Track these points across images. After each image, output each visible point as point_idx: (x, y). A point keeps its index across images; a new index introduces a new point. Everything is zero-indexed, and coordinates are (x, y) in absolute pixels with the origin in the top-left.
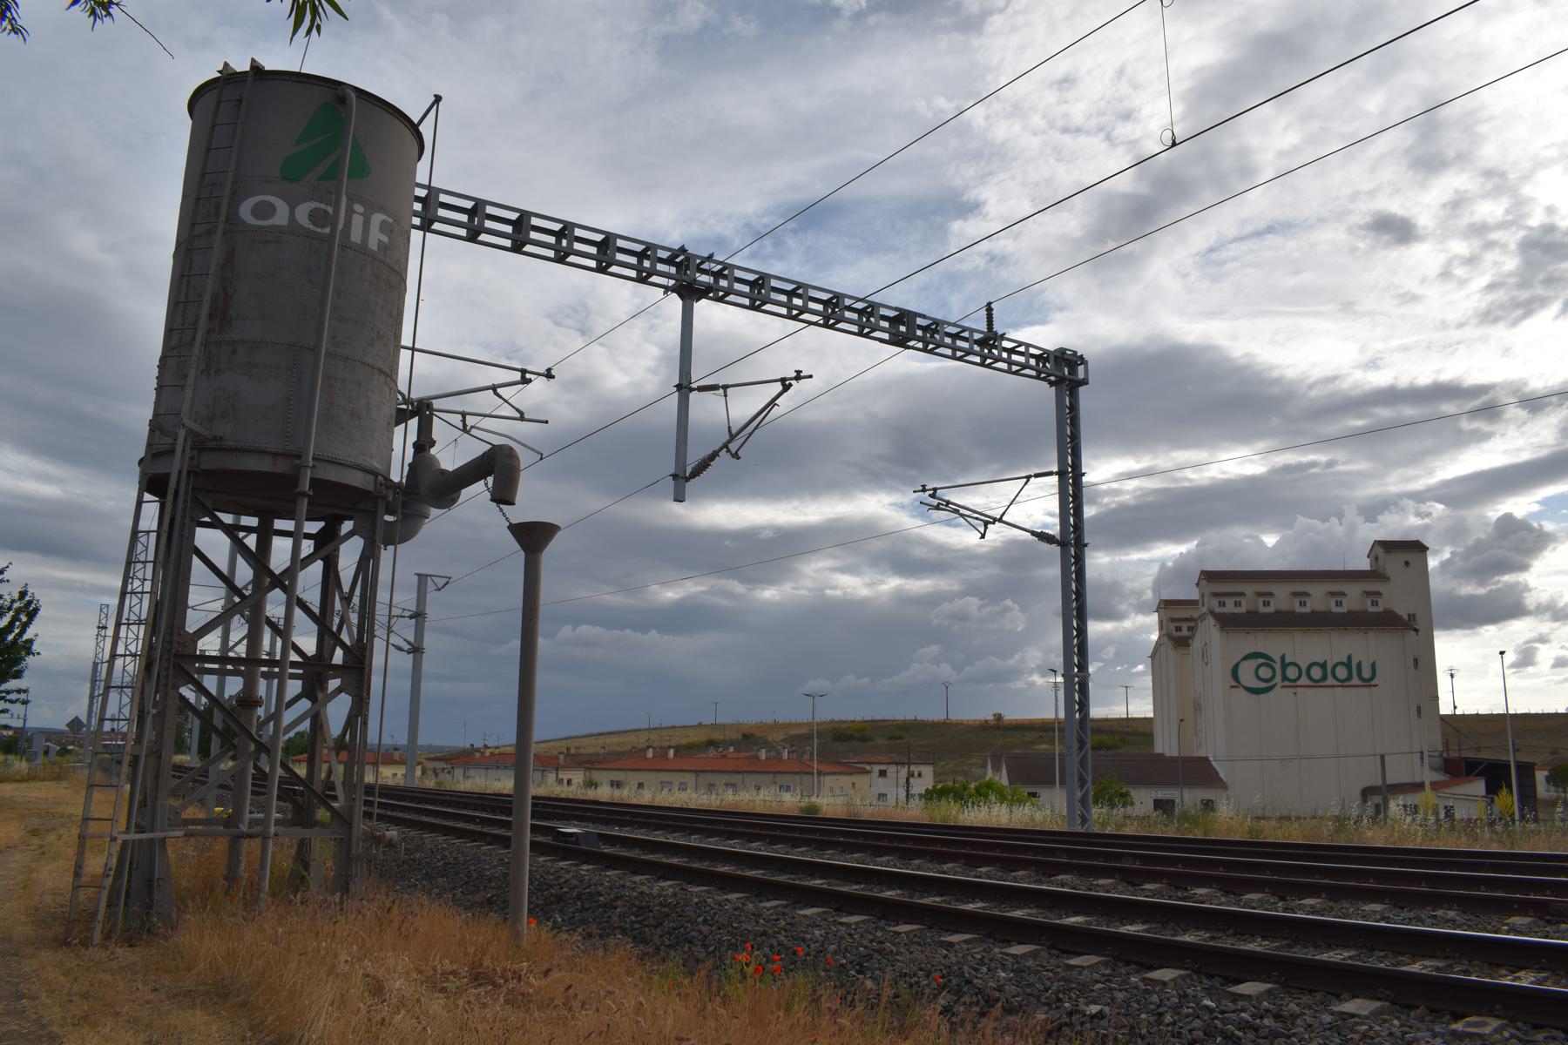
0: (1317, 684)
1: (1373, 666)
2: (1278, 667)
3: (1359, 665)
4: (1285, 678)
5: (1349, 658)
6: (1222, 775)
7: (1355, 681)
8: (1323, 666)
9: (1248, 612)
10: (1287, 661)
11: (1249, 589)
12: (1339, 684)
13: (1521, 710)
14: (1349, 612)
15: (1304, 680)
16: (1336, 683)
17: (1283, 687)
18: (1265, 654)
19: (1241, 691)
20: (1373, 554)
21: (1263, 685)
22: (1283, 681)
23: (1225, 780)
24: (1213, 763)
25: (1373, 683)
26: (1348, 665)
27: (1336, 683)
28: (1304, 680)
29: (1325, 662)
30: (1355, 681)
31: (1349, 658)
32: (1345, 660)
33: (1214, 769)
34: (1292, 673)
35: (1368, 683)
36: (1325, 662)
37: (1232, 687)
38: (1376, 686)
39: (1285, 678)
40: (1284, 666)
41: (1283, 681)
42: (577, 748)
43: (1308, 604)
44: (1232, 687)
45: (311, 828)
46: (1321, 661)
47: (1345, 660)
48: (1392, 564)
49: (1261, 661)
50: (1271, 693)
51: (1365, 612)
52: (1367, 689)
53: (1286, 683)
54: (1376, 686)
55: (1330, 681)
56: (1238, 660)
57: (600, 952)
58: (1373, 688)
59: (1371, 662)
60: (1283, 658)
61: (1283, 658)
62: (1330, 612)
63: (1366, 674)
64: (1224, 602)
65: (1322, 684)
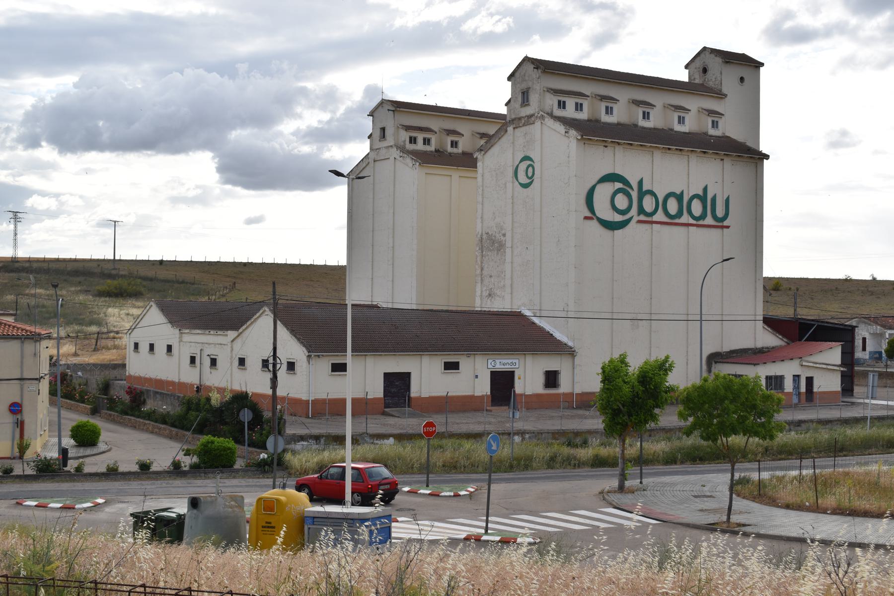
0: (672, 220)
1: (727, 201)
2: (634, 195)
3: (714, 200)
4: (641, 211)
5: (705, 189)
6: (558, 335)
7: (709, 220)
8: (679, 197)
9: (589, 120)
10: (645, 188)
11: (623, 95)
12: (694, 222)
13: (153, 259)
14: (619, 124)
15: (660, 216)
16: (692, 221)
17: (639, 222)
18: (622, 177)
19: (594, 223)
20: (698, 64)
21: (618, 218)
22: (639, 214)
23: (570, 344)
24: (536, 320)
25: (725, 223)
26: (703, 198)
27: (692, 221)
28: (660, 216)
29: (682, 193)
30: (709, 220)
31: (705, 189)
32: (701, 193)
33: (541, 330)
34: (648, 204)
35: (720, 223)
36: (682, 193)
37: (586, 218)
38: (728, 227)
39: (641, 211)
40: (642, 194)
41: (639, 214)
42: (388, 261)
43: (615, 111)
44: (586, 218)
45: (552, 335)
46: (678, 192)
47: (701, 193)
48: (728, 79)
49: (619, 185)
50: (627, 227)
51: (706, 134)
52: (719, 231)
53: (642, 217)
54: (728, 227)
55: (685, 218)
56: (594, 182)
57: (350, 545)
58: (725, 230)
59: (725, 199)
60: (640, 183)
61: (640, 183)
62: (672, 130)
63: (720, 213)
64: (564, 102)
65: (677, 221)
